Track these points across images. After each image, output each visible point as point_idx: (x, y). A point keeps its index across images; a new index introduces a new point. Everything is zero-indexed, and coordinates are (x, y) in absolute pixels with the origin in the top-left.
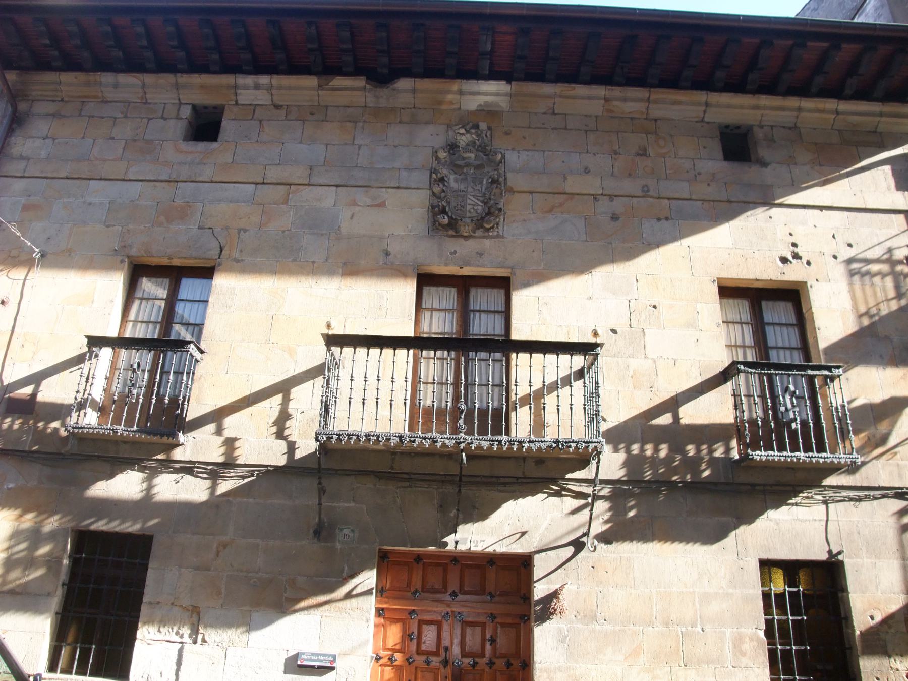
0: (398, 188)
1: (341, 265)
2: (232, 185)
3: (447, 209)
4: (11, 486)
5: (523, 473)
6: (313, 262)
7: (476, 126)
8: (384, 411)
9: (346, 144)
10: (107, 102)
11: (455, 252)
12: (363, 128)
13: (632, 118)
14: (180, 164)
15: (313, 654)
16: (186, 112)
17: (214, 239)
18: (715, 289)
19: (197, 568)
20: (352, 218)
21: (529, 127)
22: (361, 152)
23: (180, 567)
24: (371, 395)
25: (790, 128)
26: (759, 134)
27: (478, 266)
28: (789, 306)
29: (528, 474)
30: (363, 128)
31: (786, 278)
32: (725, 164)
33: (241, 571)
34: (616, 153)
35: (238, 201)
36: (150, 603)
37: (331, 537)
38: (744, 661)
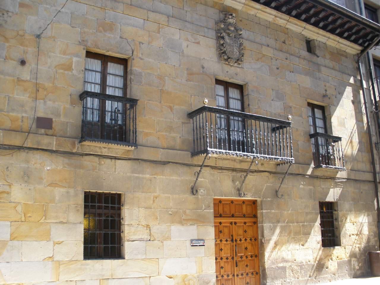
0: (204, 36)
1: (186, 69)
4: (48, 168)
19: (146, 208)
20: (187, 47)
21: (248, 20)
25: (324, 43)
27: (236, 80)
28: (122, 67)
36: (128, 225)
38: (316, 233)
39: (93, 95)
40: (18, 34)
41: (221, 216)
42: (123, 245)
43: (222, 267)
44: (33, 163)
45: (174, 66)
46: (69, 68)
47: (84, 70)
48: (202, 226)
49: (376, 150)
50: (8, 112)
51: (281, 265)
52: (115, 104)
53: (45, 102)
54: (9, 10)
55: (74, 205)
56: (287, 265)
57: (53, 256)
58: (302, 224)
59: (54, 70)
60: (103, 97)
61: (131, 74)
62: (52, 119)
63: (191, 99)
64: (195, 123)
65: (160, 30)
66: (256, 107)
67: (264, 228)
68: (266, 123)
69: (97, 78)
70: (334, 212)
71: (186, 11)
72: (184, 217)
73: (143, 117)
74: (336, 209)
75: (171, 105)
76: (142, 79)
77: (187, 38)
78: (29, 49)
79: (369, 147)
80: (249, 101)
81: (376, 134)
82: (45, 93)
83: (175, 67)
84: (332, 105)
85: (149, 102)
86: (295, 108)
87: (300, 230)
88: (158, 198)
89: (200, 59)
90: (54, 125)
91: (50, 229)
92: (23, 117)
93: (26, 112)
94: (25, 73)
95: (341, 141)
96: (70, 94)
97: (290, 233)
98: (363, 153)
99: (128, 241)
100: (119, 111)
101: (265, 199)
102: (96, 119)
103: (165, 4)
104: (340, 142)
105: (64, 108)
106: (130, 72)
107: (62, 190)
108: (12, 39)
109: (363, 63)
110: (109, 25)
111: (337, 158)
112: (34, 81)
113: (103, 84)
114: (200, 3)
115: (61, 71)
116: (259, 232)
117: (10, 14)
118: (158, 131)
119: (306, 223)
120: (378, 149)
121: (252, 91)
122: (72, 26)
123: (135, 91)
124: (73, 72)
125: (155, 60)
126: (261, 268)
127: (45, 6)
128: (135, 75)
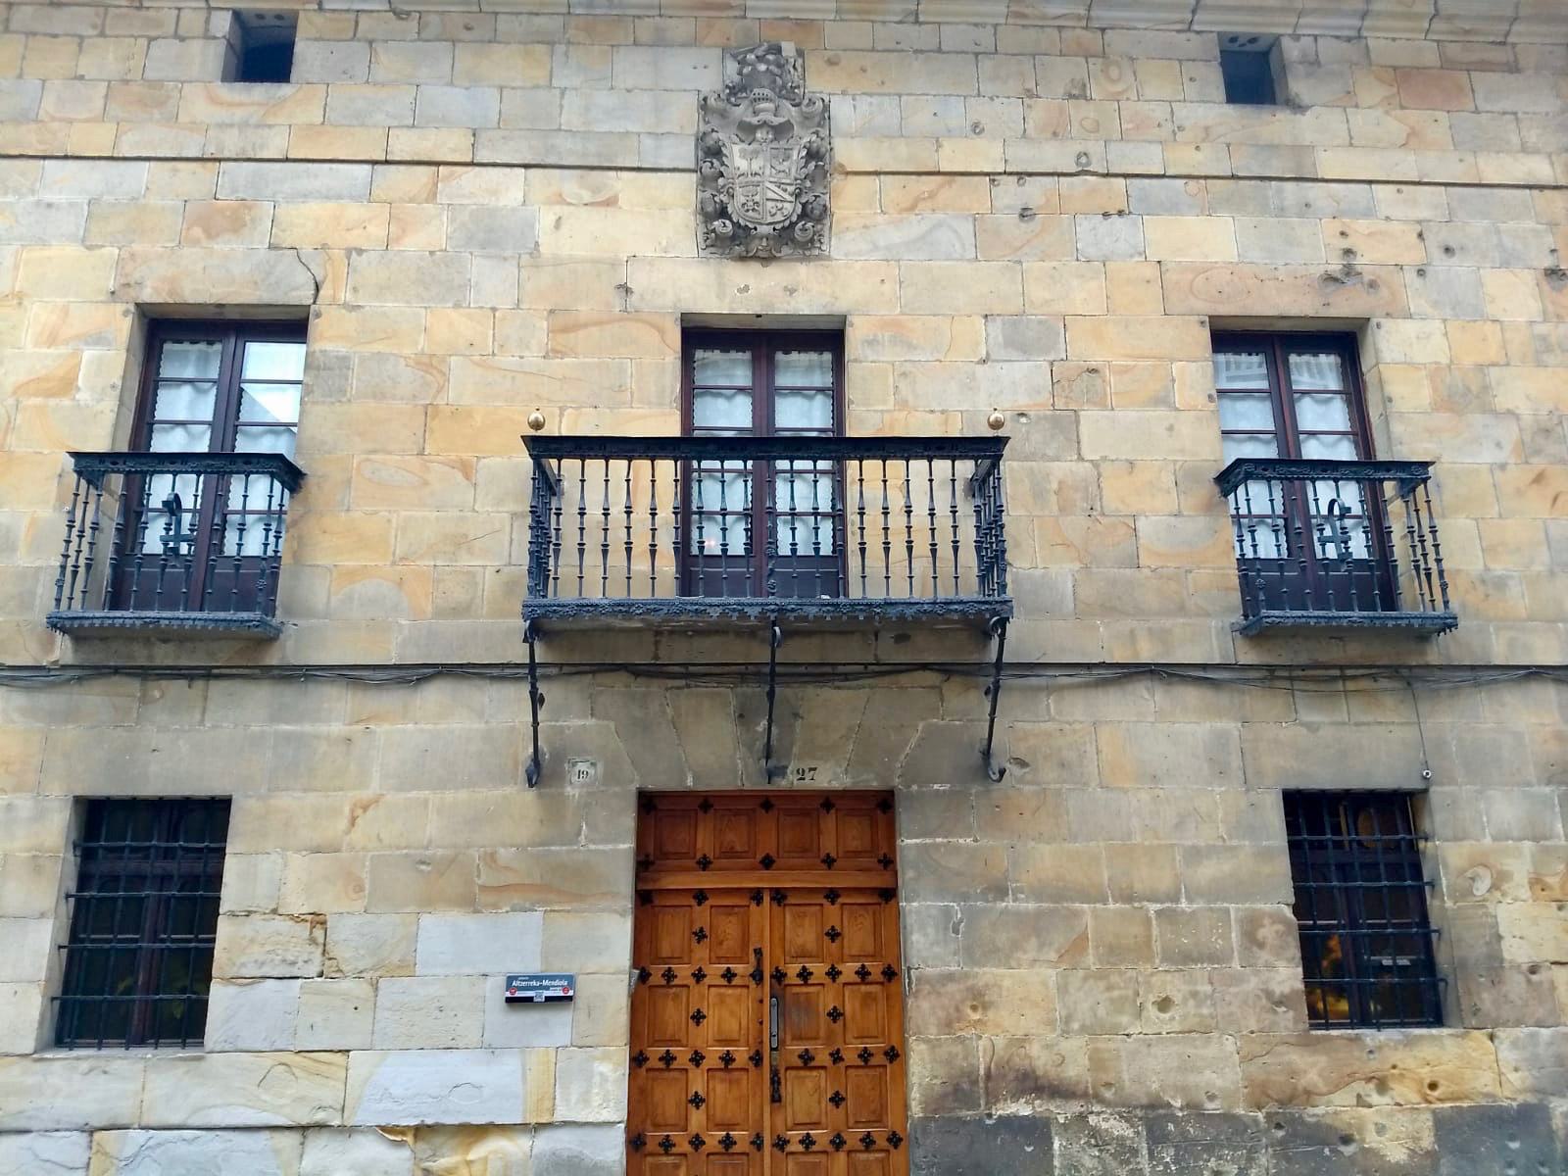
2: (327, 166)
3: (730, 210)
5: (876, 656)
6: (494, 310)
7: (778, 50)
8: (641, 565)
9: (536, 87)
11: (746, 288)
12: (566, 54)
13: (1060, 28)
14: (222, 126)
15: (532, 978)
16: (223, 23)
17: (300, 267)
18: (1205, 335)
21: (873, 50)
22: (565, 102)
23: (284, 849)
24: (617, 537)
26: (1292, 50)
29: (884, 659)
30: (566, 54)
31: (1332, 312)
32: (1231, 110)
33: (398, 848)
34: (1030, 94)
35: (340, 197)
36: (233, 914)
37: (559, 777)
38: (1264, 956)
43: (697, 1101)
46: (66, 385)
48: (569, 911)
51: (1022, 1109)
56: (1061, 1112)
58: (1159, 906)
59: (11, 401)
63: (561, 422)
66: (890, 406)
70: (1422, 844)
72: (483, 876)
75: (465, 456)
76: (347, 380)
77: (560, 195)
83: (497, 314)
85: (372, 457)
87: (1149, 937)
89: (614, 264)
96: (58, 472)
97: (1079, 945)
99: (231, 980)
101: (915, 787)
103: (467, 85)
115: (38, 400)
119: (1190, 900)
121: (871, 343)
125: (408, 302)
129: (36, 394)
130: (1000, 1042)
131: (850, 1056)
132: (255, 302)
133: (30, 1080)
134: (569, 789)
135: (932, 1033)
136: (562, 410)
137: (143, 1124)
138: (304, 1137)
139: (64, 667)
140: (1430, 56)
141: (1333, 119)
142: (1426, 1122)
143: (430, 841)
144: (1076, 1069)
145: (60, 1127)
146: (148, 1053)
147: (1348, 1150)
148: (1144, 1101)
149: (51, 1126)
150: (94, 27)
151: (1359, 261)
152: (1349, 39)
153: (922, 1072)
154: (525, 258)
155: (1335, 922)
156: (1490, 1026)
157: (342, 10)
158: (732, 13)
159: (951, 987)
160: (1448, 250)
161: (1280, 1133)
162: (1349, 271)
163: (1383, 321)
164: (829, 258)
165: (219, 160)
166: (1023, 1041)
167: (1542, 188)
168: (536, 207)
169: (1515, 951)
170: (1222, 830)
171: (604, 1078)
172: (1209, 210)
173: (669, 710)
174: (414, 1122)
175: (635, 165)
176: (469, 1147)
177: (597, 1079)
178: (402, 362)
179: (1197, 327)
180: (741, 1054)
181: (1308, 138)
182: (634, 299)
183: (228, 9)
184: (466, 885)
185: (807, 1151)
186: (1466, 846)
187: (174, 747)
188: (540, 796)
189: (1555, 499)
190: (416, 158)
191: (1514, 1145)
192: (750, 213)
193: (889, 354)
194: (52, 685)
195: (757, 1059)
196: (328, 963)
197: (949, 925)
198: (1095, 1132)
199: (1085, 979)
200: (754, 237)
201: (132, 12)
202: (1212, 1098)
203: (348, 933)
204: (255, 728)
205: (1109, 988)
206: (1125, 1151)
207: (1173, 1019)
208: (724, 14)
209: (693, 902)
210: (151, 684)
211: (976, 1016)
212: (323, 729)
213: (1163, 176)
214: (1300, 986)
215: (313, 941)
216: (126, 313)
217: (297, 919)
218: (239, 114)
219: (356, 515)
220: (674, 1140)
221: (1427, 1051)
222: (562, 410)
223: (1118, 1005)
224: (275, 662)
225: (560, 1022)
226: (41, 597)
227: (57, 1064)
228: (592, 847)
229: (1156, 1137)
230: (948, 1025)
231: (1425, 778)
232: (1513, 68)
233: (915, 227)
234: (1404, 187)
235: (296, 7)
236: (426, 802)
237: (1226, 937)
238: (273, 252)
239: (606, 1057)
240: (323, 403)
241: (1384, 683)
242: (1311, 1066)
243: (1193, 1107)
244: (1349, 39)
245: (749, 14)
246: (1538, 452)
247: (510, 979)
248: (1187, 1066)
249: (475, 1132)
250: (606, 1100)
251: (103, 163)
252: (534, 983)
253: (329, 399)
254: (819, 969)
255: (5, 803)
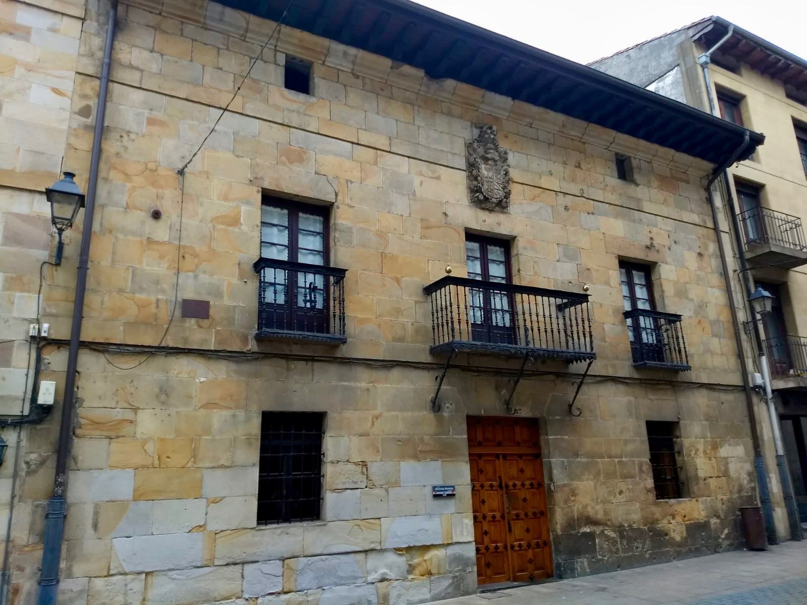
4: (202, 379)
10: (206, 29)
13: (572, 139)
15: (441, 487)
16: (282, 60)
17: (329, 185)
18: (617, 261)
24: (444, 312)
30: (418, 111)
33: (390, 435)
36: (332, 462)
38: (644, 475)
39: (275, 264)
40: (147, 168)
41: (480, 444)
42: (323, 499)
43: (486, 533)
44: (176, 372)
45: (402, 216)
47: (260, 224)
49: (746, 333)
50: (133, 293)
51: (587, 530)
52: (310, 277)
53: (196, 277)
54: (131, 130)
55: (245, 435)
56: (598, 530)
57: (206, 522)
59: (210, 225)
60: (293, 266)
61: (335, 230)
62: (208, 302)
64: (434, 302)
65: (378, 159)
66: (532, 273)
67: (553, 465)
68: (545, 298)
69: (282, 238)
70: (675, 439)
71: (419, 127)
73: (356, 295)
74: (678, 434)
77: (421, 172)
78: (166, 192)
79: (732, 329)
80: (519, 265)
81: (745, 307)
82: (196, 261)
84: (662, 262)
86: (597, 271)
88: (379, 419)
90: (211, 312)
91: (201, 481)
92: (158, 300)
93: (163, 291)
94: (161, 231)
95: (680, 321)
97: (598, 474)
98: (722, 340)
99: (334, 490)
100: (315, 288)
101: (550, 417)
102: (281, 299)
104: (678, 323)
105: (229, 284)
106: (334, 226)
107: (227, 413)
108: (137, 175)
109: (718, 189)
110: (296, 153)
111: (675, 349)
112: (176, 243)
113: (293, 247)
114: (440, 111)
116: (545, 473)
117: (133, 136)
118: (379, 316)
119: (626, 458)
120: (749, 332)
121: (525, 248)
122: (236, 154)
123: (341, 257)
124: (242, 228)
126: (551, 534)
127: (190, 122)
128: (340, 231)
129: (223, 223)
130: (580, 507)
131: (530, 514)
132: (313, 197)
133: (256, 539)
134: (444, 413)
135: (562, 505)
136: (428, 260)
137: (305, 554)
138: (366, 555)
139: (253, 353)
140: (668, 174)
141: (645, 190)
142: (684, 528)
143: (401, 432)
144: (600, 516)
145: (270, 559)
146: (305, 524)
147: (667, 538)
148: (618, 525)
149: (267, 559)
150: (224, 45)
151: (655, 243)
152: (648, 162)
153: (559, 518)
154: (411, 196)
155: (266, 474)
156: (696, 497)
157: (331, 67)
158: (474, 108)
159: (566, 489)
160: (675, 242)
161: (651, 534)
162: (652, 244)
163: (661, 264)
164: (510, 214)
165: (290, 127)
166: (586, 506)
167: (696, 225)
168: (413, 175)
169: (701, 474)
170: (632, 435)
171: (467, 524)
172: (616, 217)
173: (474, 385)
174: (406, 546)
175: (446, 165)
176: (423, 555)
177: (465, 526)
178: (371, 233)
179: (614, 259)
180: (498, 515)
181: (640, 196)
182: (449, 219)
183: (283, 53)
184: (413, 450)
185: (521, 550)
186: (689, 439)
187: (304, 390)
188: (435, 416)
189: (703, 329)
190: (369, 145)
191: (703, 534)
192: (489, 193)
193: (531, 254)
194: (248, 361)
195: (503, 517)
196: (369, 482)
197: (564, 467)
198: (607, 536)
199: (601, 484)
200: (490, 202)
201: (240, 41)
202: (634, 523)
203: (375, 469)
204: (334, 383)
205: (607, 487)
206: (614, 542)
207: (623, 497)
208: (471, 108)
209: (477, 458)
210: (290, 362)
211: (573, 499)
212: (359, 385)
213: (603, 202)
214: (653, 485)
215: (363, 473)
216: (258, 191)
217: (356, 464)
218: (295, 106)
219: (361, 296)
220: (480, 548)
221: (683, 506)
222: (428, 260)
223: (610, 493)
224: (339, 356)
225: (451, 503)
226: (238, 320)
227: (266, 532)
228: (455, 436)
229: (622, 537)
230: (566, 502)
231: (679, 418)
232: (688, 182)
233: (534, 207)
234: (664, 219)
235: (313, 60)
236: (397, 416)
237: (634, 470)
238: (317, 175)
239: (467, 517)
240: (344, 246)
241: (668, 387)
242: (657, 511)
243: (630, 526)
244: (648, 162)
245: (479, 110)
246: (699, 314)
247: (434, 487)
248: (628, 513)
249: (426, 548)
250: (468, 533)
251: (237, 115)
252: (442, 489)
253: (346, 245)
254: (518, 483)
255: (232, 414)
